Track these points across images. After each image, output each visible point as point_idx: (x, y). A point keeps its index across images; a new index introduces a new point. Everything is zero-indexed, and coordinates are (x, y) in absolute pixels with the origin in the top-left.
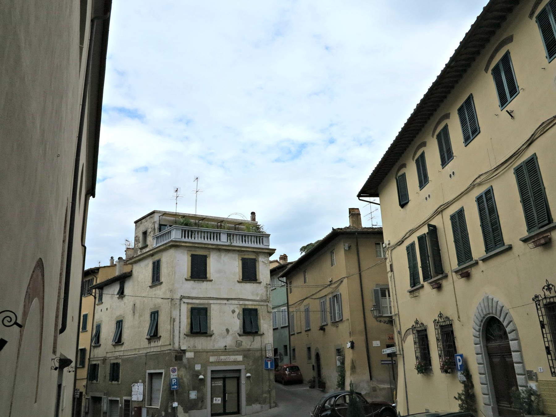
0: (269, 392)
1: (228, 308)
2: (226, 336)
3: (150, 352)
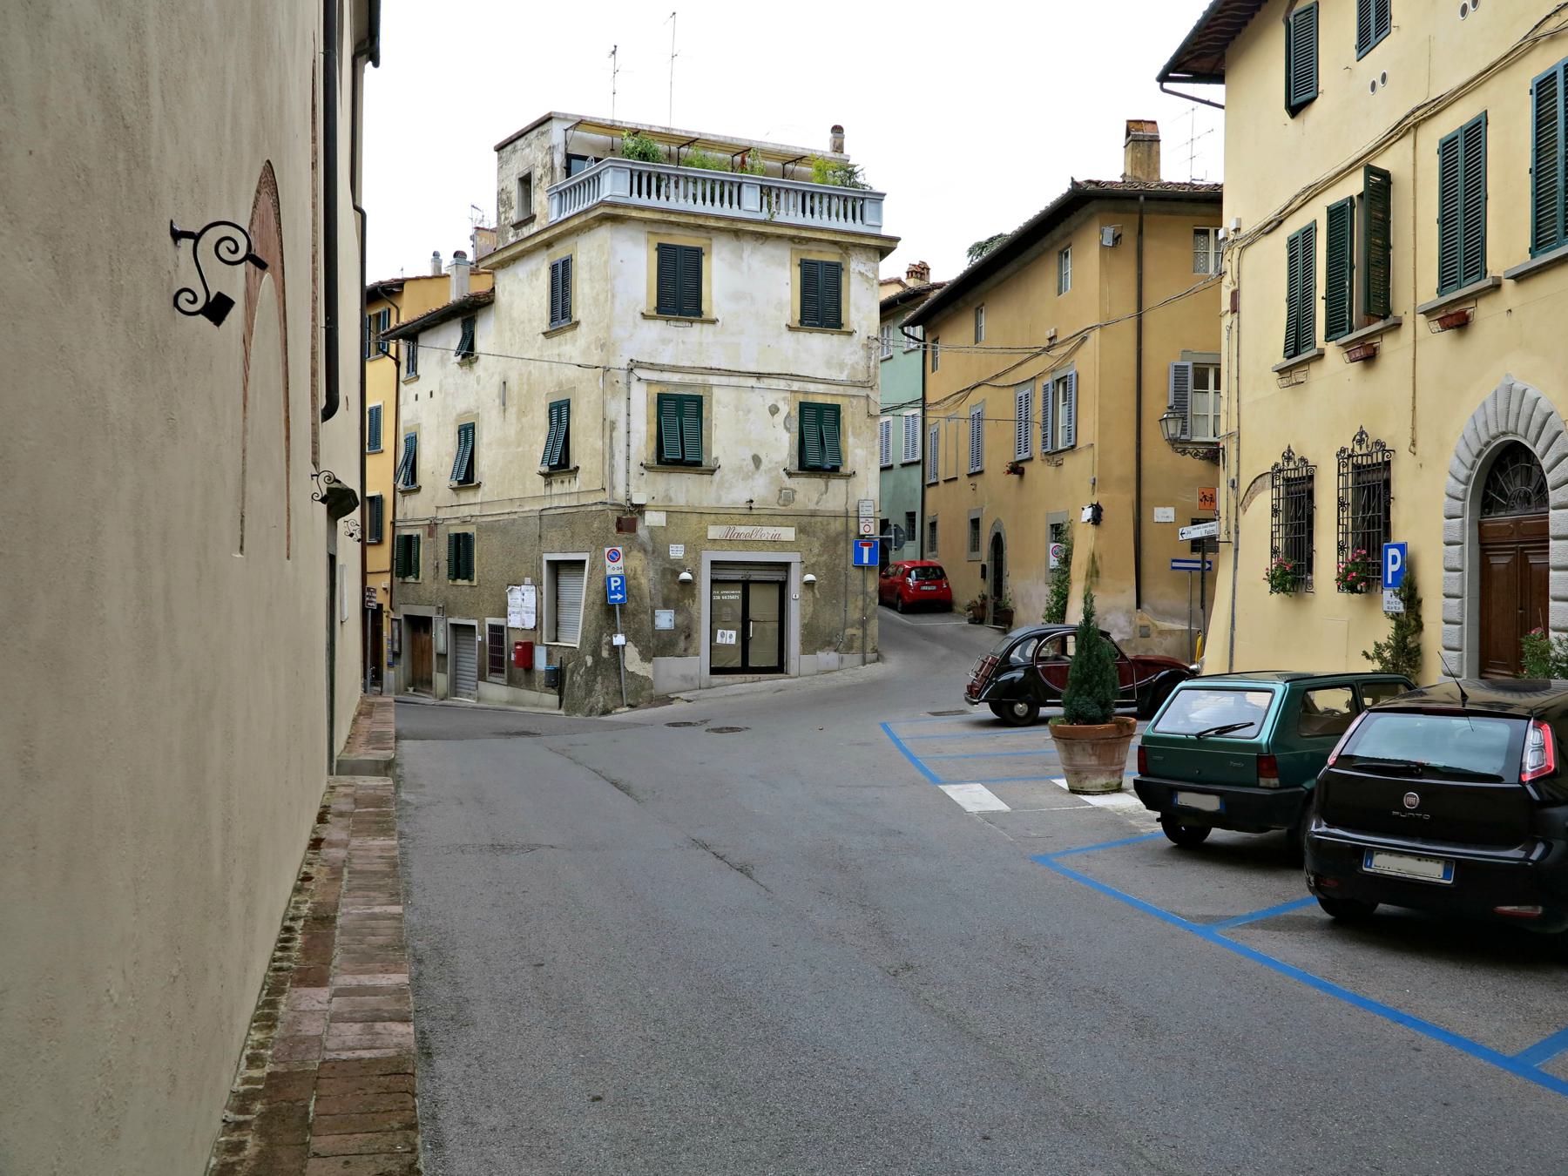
0: (863, 624)
1: (760, 400)
2: (753, 474)
3: (550, 508)
